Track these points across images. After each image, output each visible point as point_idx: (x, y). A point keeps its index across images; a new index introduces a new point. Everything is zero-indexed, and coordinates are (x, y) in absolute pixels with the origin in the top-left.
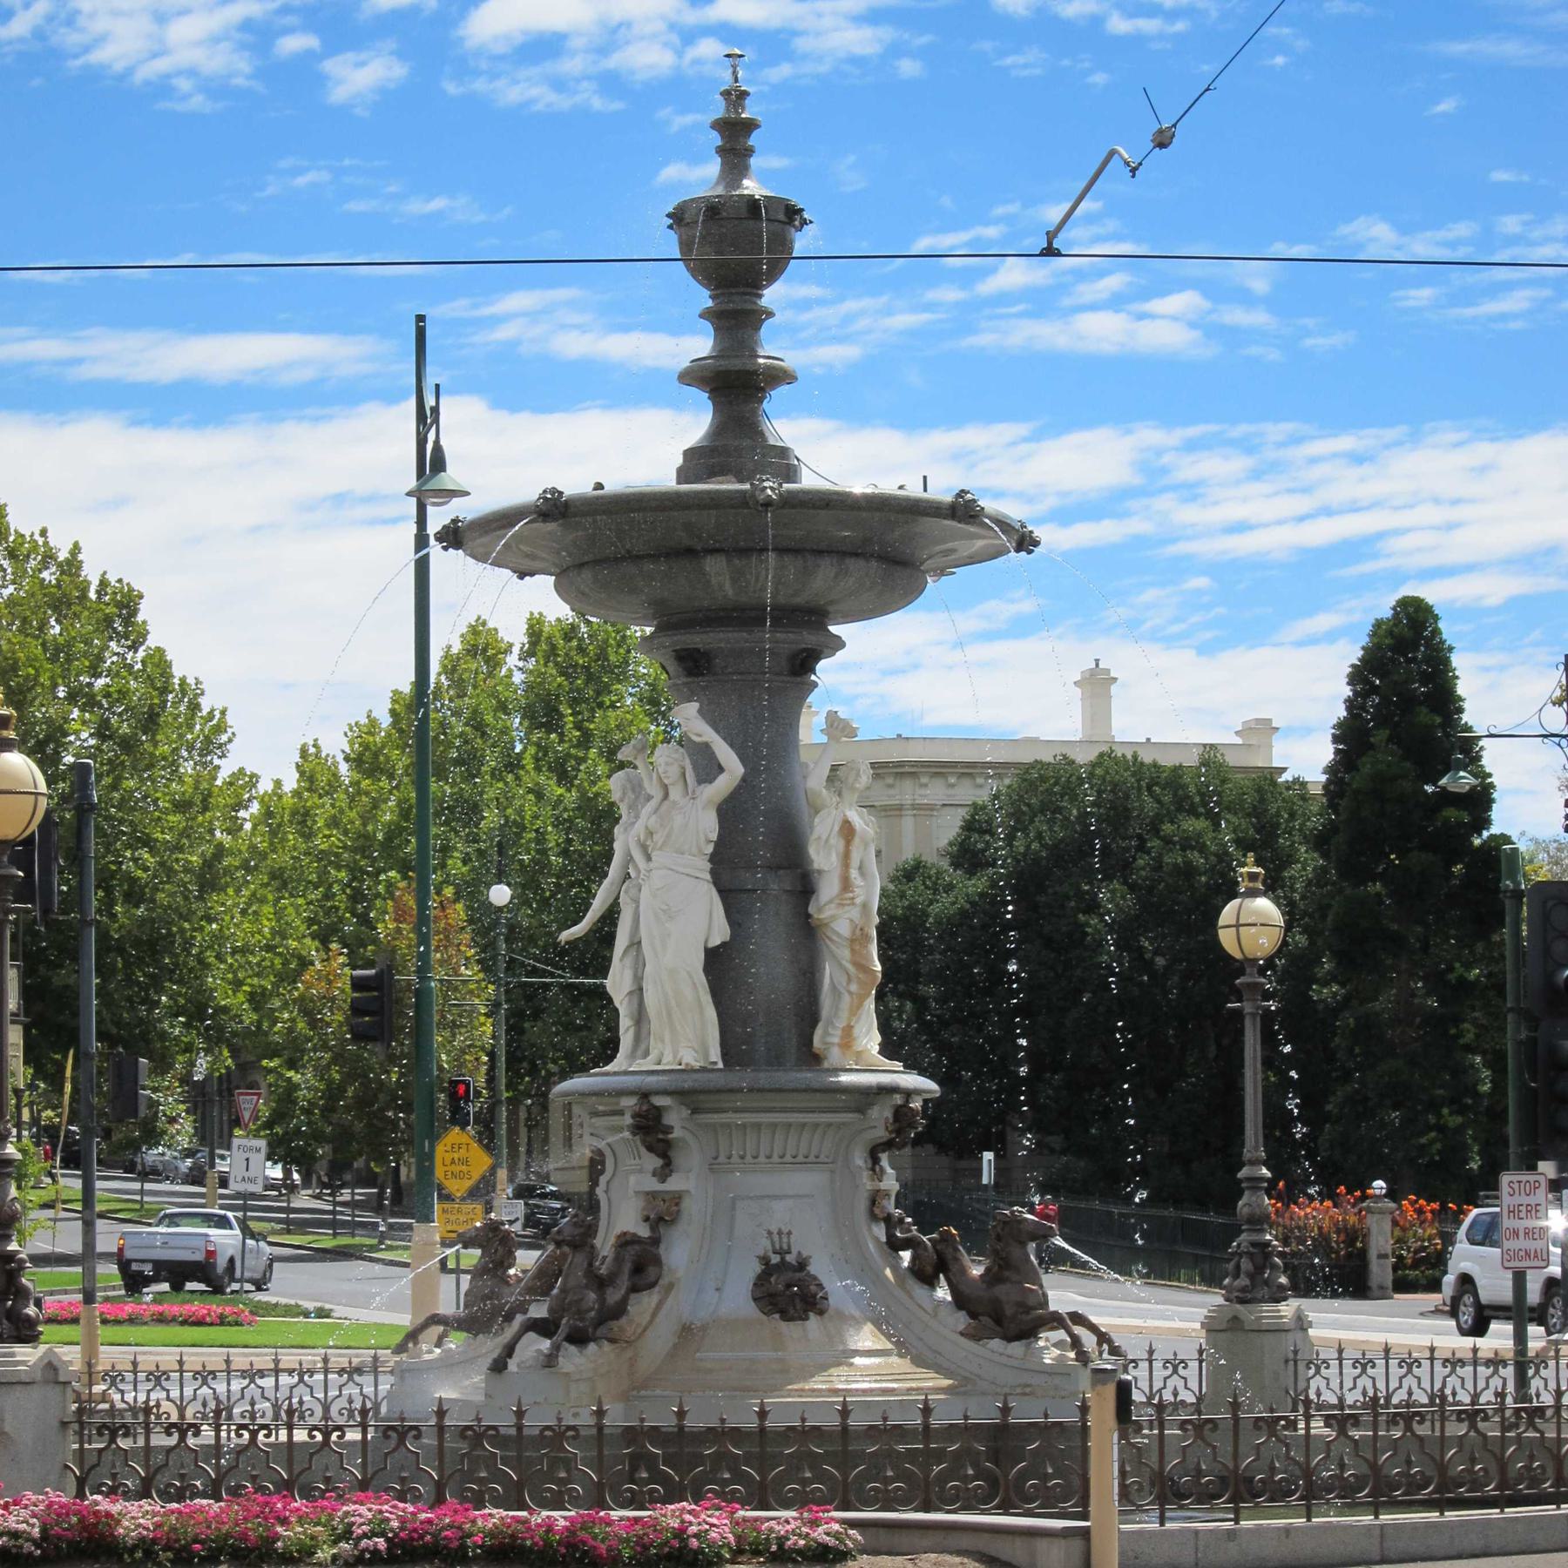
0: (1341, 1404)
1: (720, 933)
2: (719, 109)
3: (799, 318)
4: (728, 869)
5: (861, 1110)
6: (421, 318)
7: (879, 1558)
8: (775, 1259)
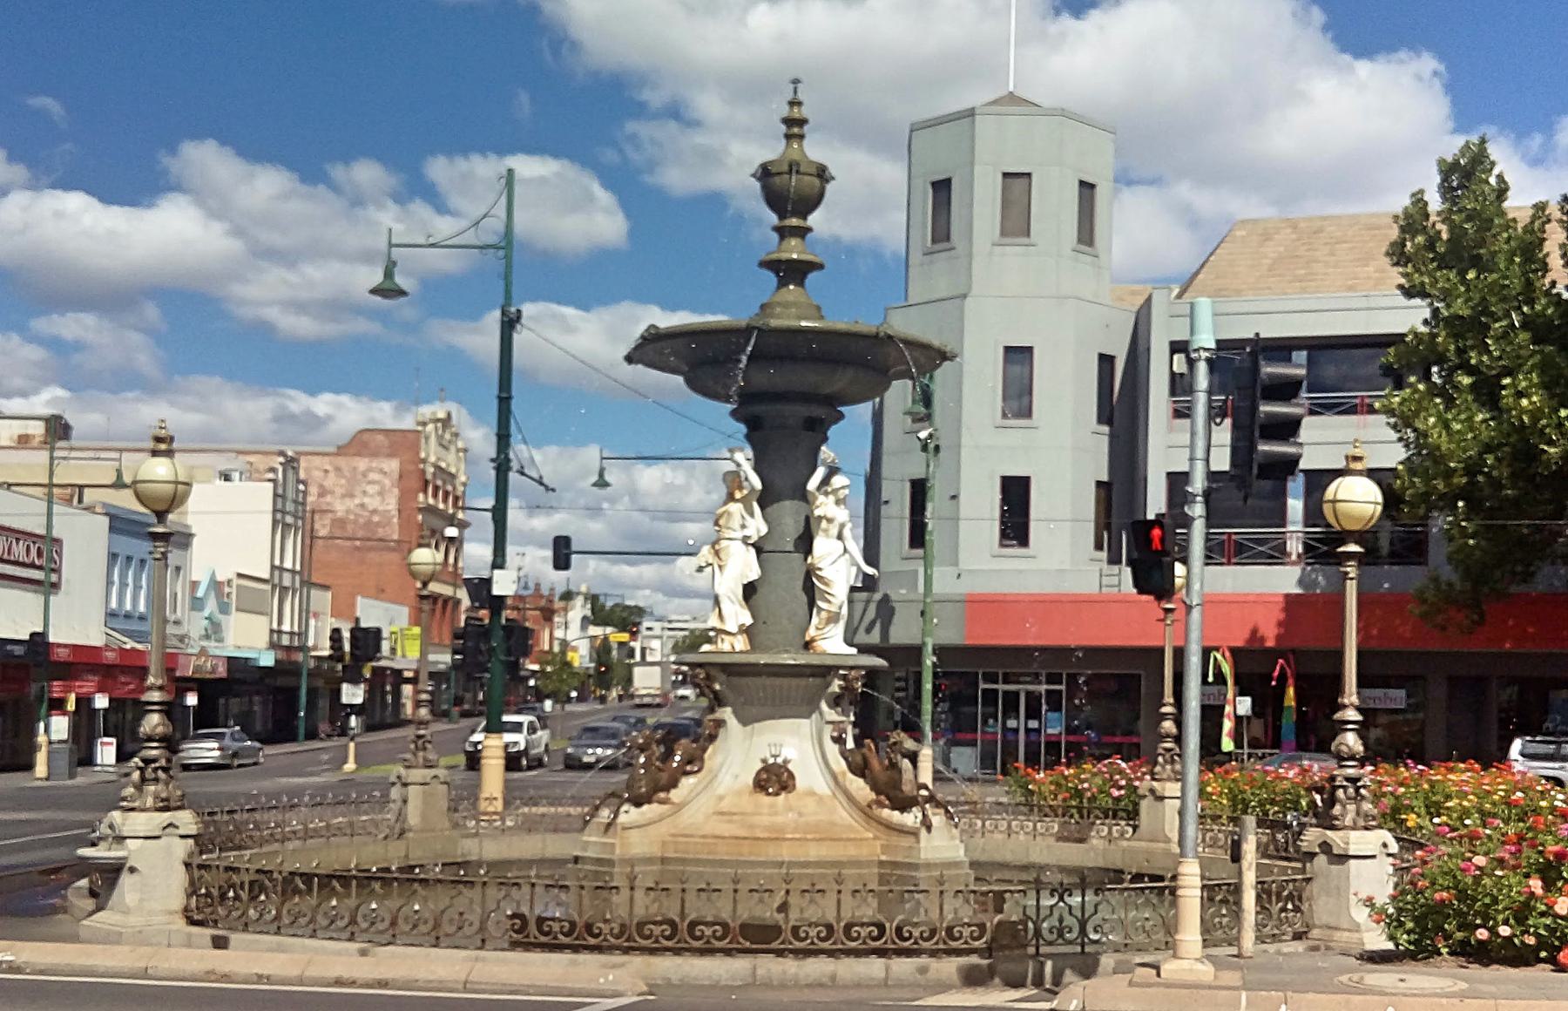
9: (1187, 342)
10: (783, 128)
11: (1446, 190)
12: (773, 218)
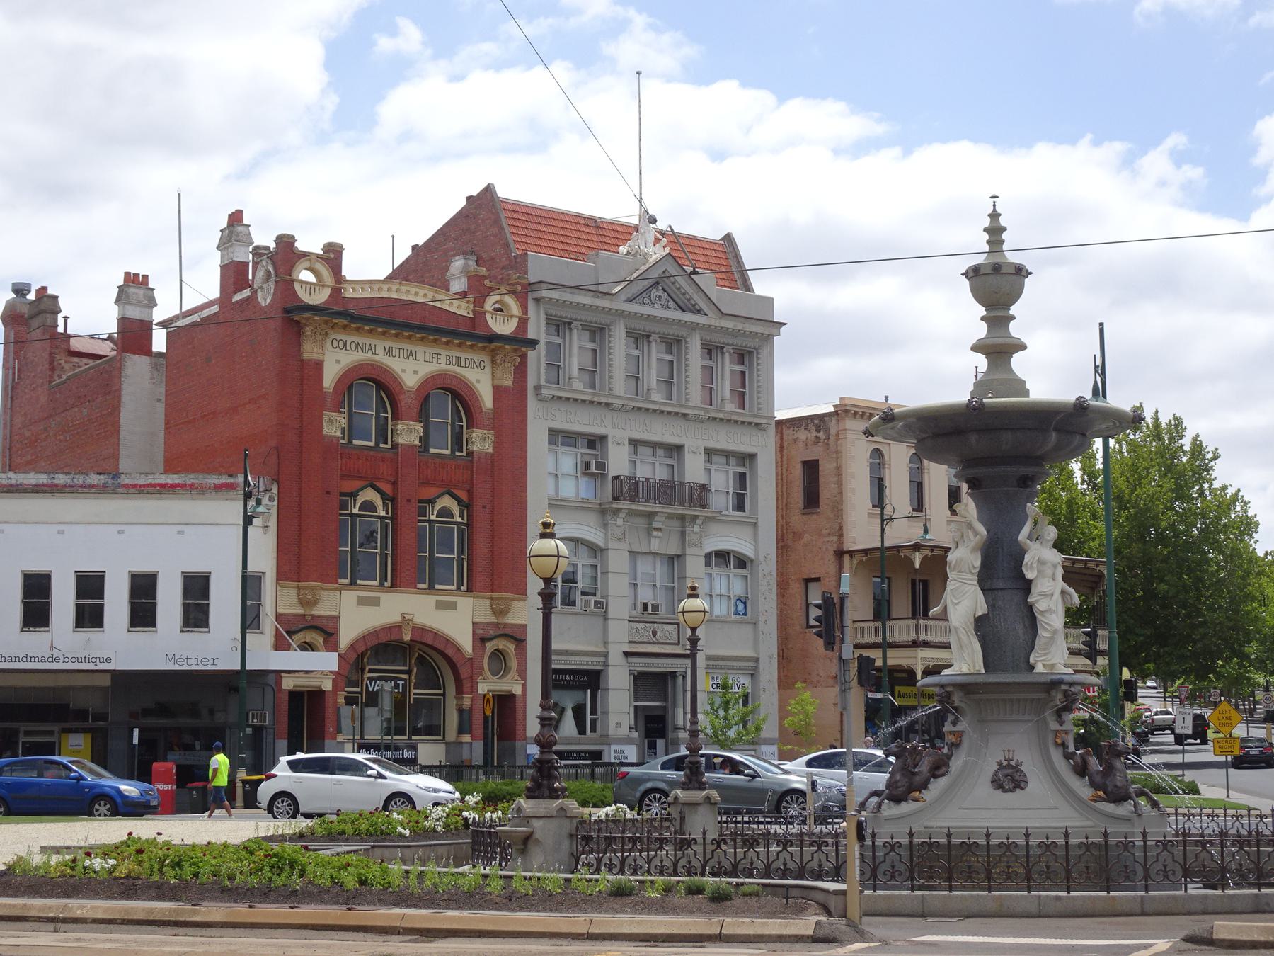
0: (1202, 835)
1: (982, 609)
2: (987, 222)
3: (1025, 317)
4: (986, 579)
5: (1048, 692)
6: (1101, 325)
7: (779, 932)
8: (1005, 763)
12: (982, 311)
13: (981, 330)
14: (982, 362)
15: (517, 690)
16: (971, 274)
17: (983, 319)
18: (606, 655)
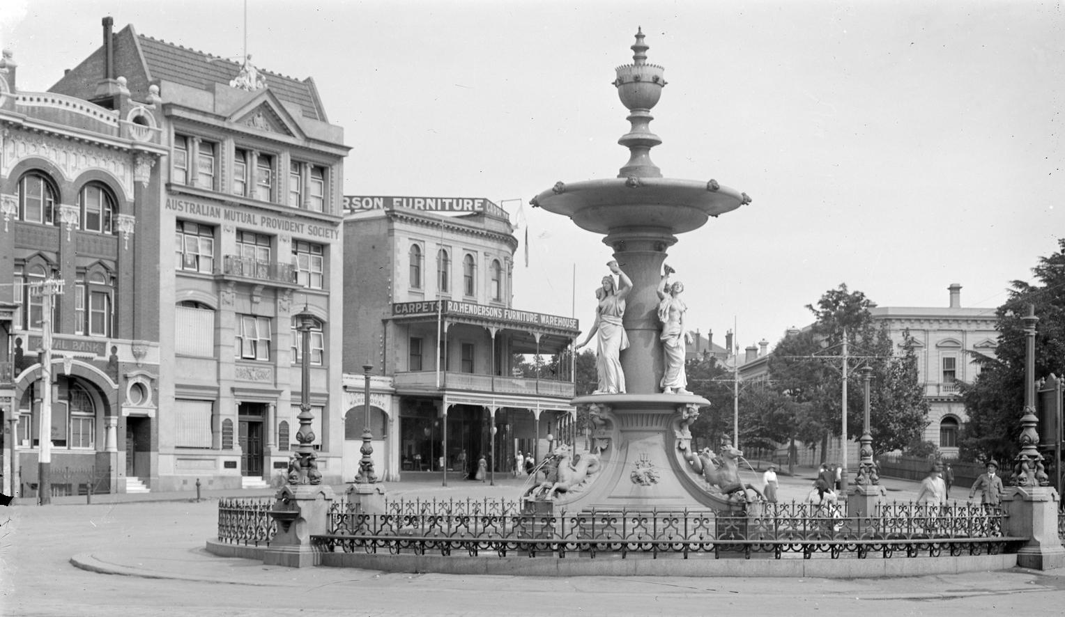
9: (796, 462)
10: (633, 53)
11: (875, 427)
12: (628, 112)
13: (626, 128)
14: (626, 152)
15: (152, 414)
16: (618, 83)
17: (629, 118)
18: (218, 389)
